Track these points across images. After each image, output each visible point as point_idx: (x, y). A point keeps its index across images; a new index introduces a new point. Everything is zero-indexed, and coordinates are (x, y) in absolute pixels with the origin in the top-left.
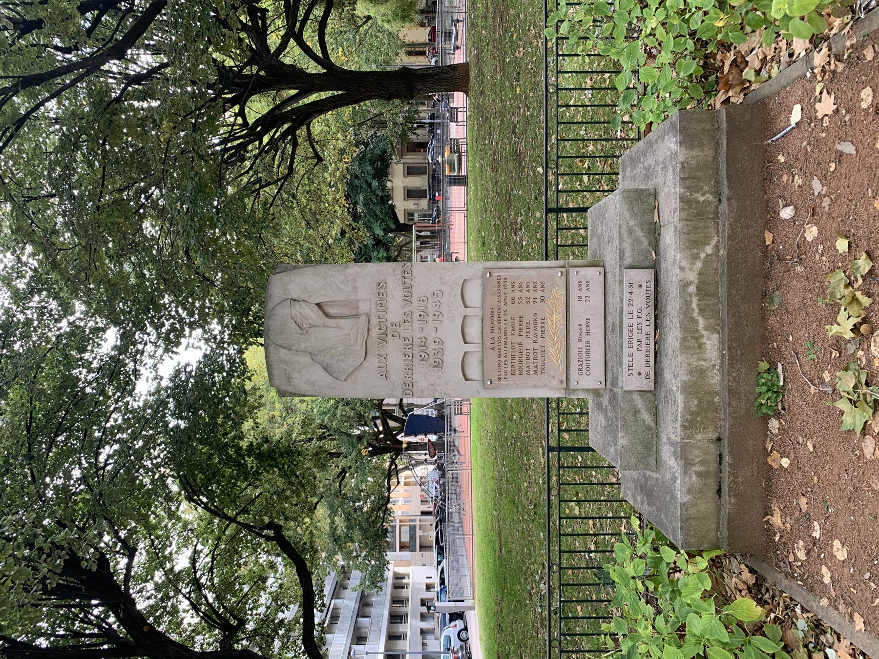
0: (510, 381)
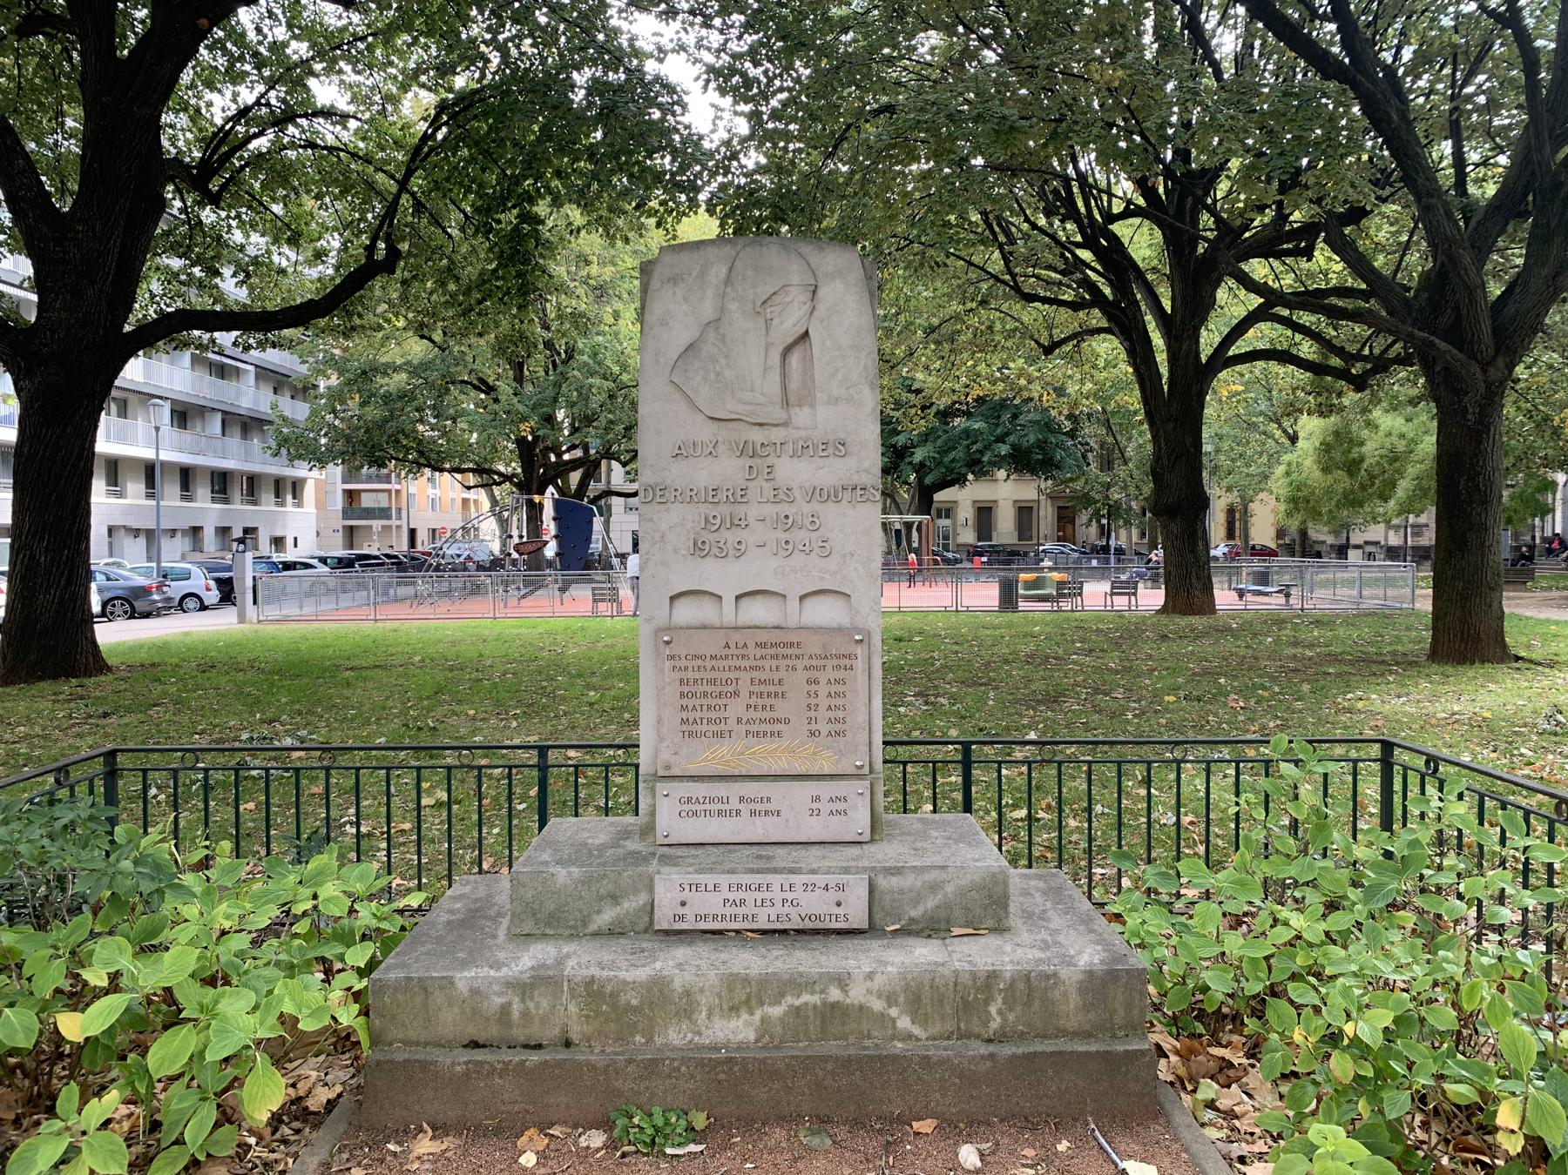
0: (670, 676)
